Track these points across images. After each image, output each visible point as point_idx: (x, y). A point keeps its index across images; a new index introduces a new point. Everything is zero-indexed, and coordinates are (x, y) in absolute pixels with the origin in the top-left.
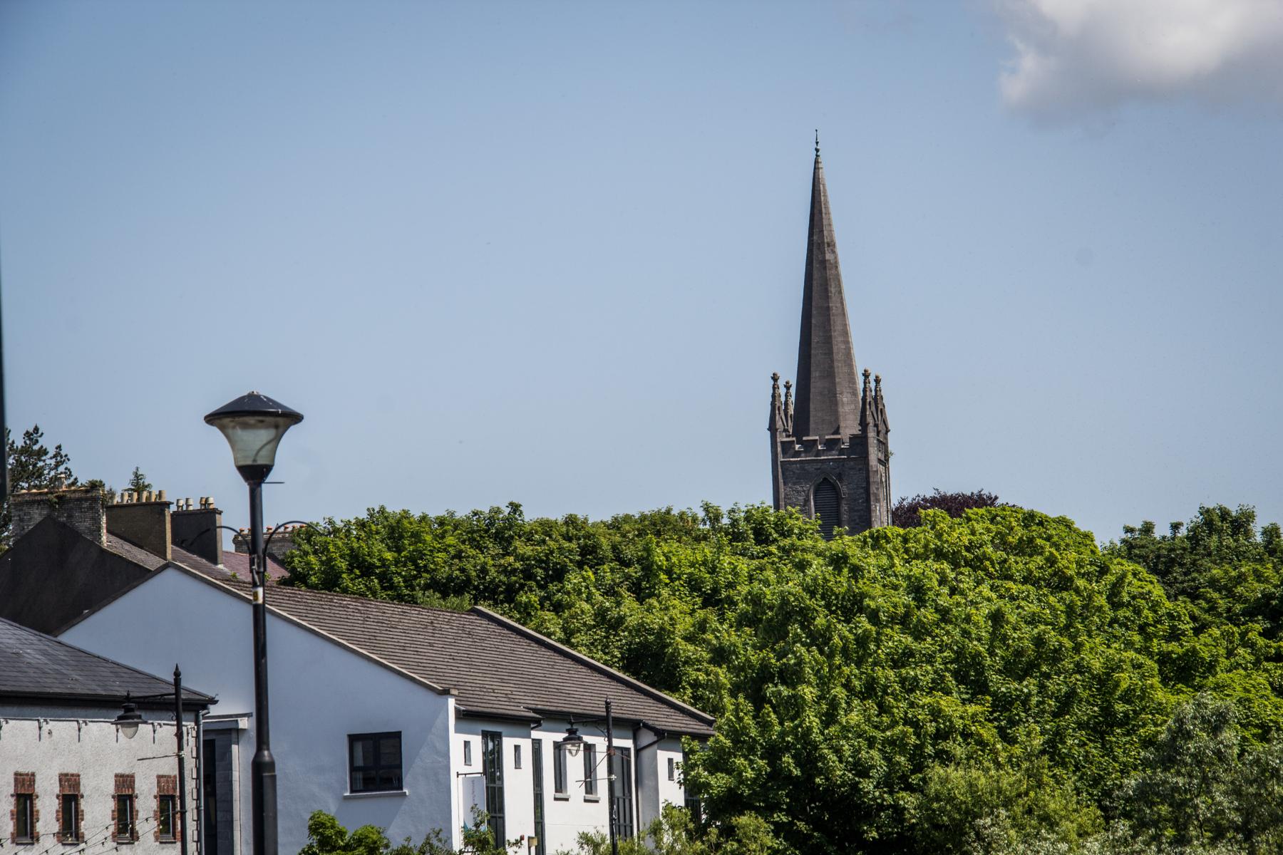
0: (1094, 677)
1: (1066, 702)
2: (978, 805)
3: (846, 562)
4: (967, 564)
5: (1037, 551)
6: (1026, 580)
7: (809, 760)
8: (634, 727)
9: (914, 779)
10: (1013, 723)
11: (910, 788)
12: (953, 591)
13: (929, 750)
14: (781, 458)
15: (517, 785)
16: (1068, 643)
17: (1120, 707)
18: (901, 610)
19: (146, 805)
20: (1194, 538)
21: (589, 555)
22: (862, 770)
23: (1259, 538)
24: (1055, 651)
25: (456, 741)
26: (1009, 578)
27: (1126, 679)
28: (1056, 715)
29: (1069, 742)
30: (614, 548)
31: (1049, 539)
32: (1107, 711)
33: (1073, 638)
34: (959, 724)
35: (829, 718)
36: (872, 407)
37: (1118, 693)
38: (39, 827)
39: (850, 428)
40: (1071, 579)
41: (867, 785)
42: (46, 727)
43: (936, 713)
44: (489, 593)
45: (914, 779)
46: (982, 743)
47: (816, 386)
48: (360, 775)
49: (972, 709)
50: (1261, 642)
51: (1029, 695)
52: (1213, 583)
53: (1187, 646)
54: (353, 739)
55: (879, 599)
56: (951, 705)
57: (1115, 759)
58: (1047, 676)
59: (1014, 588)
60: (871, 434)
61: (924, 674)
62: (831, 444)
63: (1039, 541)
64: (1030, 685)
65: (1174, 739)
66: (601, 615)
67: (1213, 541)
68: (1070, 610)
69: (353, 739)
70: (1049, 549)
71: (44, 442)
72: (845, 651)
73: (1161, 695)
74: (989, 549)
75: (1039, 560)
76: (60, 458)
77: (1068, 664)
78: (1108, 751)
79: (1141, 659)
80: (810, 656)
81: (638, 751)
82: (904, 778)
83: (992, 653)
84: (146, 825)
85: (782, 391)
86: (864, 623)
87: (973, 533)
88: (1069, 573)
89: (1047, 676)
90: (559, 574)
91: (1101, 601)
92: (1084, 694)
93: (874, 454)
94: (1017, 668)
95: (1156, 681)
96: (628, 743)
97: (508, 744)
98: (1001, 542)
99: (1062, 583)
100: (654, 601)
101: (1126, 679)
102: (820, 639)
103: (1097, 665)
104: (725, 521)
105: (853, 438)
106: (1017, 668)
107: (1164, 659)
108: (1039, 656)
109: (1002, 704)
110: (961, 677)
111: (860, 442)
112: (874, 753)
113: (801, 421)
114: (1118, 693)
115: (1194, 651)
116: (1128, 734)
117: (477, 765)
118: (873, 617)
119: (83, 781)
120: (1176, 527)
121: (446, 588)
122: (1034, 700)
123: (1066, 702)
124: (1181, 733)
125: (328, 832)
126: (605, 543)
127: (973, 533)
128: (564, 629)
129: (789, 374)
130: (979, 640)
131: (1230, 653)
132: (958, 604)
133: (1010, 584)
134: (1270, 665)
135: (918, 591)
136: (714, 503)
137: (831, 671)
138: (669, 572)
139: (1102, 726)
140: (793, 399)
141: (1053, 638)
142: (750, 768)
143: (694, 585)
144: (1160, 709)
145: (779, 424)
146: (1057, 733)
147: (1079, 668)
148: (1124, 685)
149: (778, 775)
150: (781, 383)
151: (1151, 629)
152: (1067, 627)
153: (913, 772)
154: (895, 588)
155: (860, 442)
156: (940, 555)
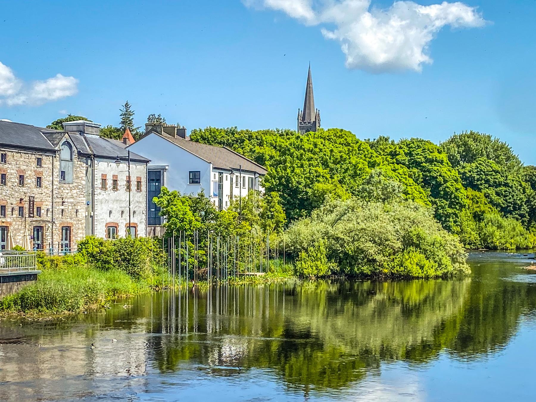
0: (353, 165)
1: (346, 170)
2: (324, 193)
3: (299, 138)
4: (328, 140)
5: (343, 137)
6: (340, 144)
7: (288, 180)
8: (255, 173)
9: (311, 186)
10: (334, 174)
11: (310, 188)
12: (324, 146)
13: (315, 179)
14: (299, 125)
15: (226, 185)
16: (348, 157)
17: (358, 172)
18: (311, 149)
19: (110, 183)
20: (378, 142)
21: (250, 138)
22: (299, 183)
23: (390, 142)
24: (345, 159)
25: (212, 174)
26: (336, 143)
27: (360, 166)
28: (344, 173)
29: (346, 179)
30: (256, 137)
31: (346, 135)
32: (355, 172)
33: (349, 156)
34: (322, 174)
35: (293, 171)
36: (317, 116)
37: (358, 169)
38: (107, 186)
39: (313, 120)
40: (350, 144)
41: (300, 186)
42: (109, 164)
43: (316, 171)
44: (230, 145)
45: (311, 186)
46: (327, 179)
47: (307, 111)
48: (191, 180)
49: (325, 171)
50: (390, 160)
51: (338, 168)
52: (381, 149)
53: (374, 160)
54: (190, 172)
55: (307, 146)
56: (321, 170)
57: (356, 183)
58: (343, 164)
59: (337, 145)
60: (317, 120)
61: (314, 163)
62: (309, 123)
63: (343, 135)
64: (338, 166)
65: (370, 178)
66: (251, 149)
67: (381, 142)
68: (349, 149)
69: (190, 172)
70: (345, 137)
71: (162, 117)
72: (297, 157)
73: (368, 169)
74: (332, 137)
75: (343, 139)
76: (164, 120)
77: (347, 162)
78: (355, 181)
79: (364, 162)
80: (289, 158)
81: (255, 178)
82: (309, 185)
83: (330, 159)
84: (134, 187)
85: (300, 112)
86: (302, 151)
87: (329, 133)
88: (349, 142)
89: (343, 164)
90: (243, 141)
91: (356, 148)
92: (351, 169)
93: (317, 125)
94: (335, 162)
95: (367, 167)
96: (253, 176)
97: (224, 175)
98: (335, 135)
99: (348, 145)
100: (262, 147)
101: (360, 166)
102: (291, 155)
103: (354, 163)
104: (280, 132)
105: (313, 122)
106: (335, 162)
107: (369, 162)
108: (341, 160)
109: (332, 170)
110: (323, 164)
111: (315, 122)
112: (302, 179)
113: (304, 118)
114: (358, 169)
115: (375, 161)
116: (360, 178)
117: (217, 179)
118: (304, 150)
119: (118, 177)
120: (374, 139)
121: (220, 143)
122: (339, 169)
123: (346, 170)
124: (371, 177)
125: (165, 191)
126: (254, 136)
127: (329, 133)
128: (243, 152)
129: (302, 109)
130: (328, 156)
131: (383, 162)
132: (324, 148)
133: (336, 144)
134: (391, 165)
135: (315, 145)
136: (278, 128)
137: (293, 161)
138: (266, 142)
139: (354, 176)
140: (302, 114)
141: (345, 156)
142: (275, 182)
143: (271, 145)
144: (367, 173)
145: (299, 119)
146: (344, 177)
147: (350, 163)
148: (359, 167)
149: (280, 184)
150: (300, 110)
151: (367, 156)
152: (348, 154)
153: (311, 184)
154: (310, 144)
155: (315, 122)
156: (321, 138)
